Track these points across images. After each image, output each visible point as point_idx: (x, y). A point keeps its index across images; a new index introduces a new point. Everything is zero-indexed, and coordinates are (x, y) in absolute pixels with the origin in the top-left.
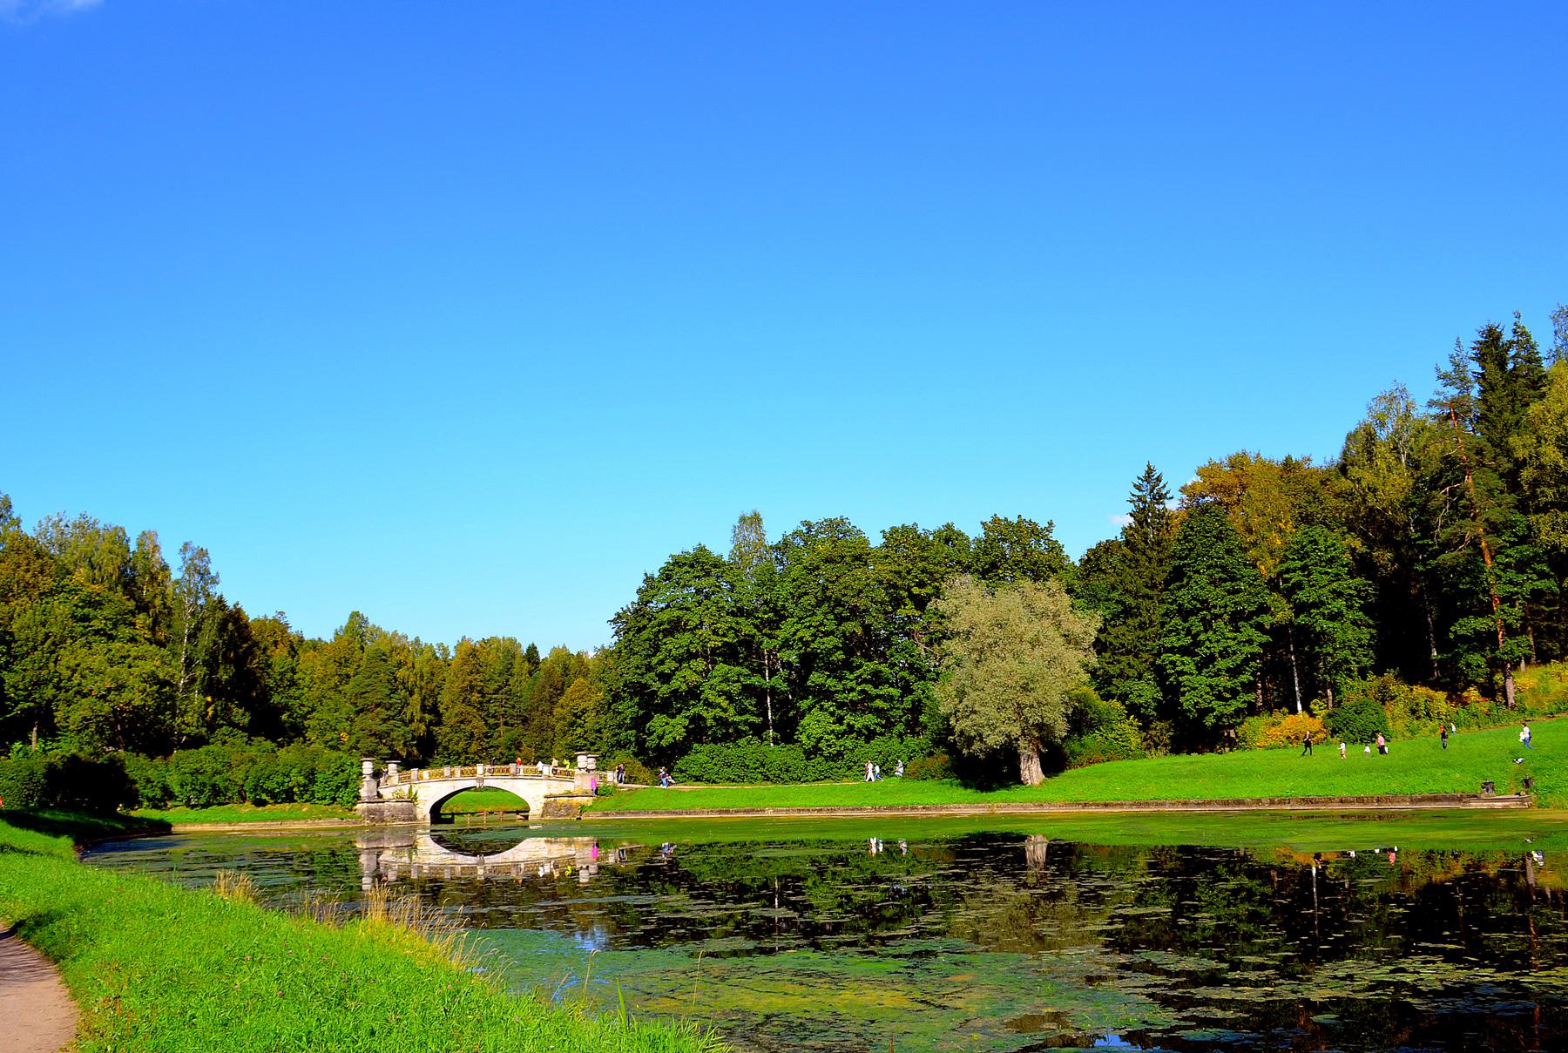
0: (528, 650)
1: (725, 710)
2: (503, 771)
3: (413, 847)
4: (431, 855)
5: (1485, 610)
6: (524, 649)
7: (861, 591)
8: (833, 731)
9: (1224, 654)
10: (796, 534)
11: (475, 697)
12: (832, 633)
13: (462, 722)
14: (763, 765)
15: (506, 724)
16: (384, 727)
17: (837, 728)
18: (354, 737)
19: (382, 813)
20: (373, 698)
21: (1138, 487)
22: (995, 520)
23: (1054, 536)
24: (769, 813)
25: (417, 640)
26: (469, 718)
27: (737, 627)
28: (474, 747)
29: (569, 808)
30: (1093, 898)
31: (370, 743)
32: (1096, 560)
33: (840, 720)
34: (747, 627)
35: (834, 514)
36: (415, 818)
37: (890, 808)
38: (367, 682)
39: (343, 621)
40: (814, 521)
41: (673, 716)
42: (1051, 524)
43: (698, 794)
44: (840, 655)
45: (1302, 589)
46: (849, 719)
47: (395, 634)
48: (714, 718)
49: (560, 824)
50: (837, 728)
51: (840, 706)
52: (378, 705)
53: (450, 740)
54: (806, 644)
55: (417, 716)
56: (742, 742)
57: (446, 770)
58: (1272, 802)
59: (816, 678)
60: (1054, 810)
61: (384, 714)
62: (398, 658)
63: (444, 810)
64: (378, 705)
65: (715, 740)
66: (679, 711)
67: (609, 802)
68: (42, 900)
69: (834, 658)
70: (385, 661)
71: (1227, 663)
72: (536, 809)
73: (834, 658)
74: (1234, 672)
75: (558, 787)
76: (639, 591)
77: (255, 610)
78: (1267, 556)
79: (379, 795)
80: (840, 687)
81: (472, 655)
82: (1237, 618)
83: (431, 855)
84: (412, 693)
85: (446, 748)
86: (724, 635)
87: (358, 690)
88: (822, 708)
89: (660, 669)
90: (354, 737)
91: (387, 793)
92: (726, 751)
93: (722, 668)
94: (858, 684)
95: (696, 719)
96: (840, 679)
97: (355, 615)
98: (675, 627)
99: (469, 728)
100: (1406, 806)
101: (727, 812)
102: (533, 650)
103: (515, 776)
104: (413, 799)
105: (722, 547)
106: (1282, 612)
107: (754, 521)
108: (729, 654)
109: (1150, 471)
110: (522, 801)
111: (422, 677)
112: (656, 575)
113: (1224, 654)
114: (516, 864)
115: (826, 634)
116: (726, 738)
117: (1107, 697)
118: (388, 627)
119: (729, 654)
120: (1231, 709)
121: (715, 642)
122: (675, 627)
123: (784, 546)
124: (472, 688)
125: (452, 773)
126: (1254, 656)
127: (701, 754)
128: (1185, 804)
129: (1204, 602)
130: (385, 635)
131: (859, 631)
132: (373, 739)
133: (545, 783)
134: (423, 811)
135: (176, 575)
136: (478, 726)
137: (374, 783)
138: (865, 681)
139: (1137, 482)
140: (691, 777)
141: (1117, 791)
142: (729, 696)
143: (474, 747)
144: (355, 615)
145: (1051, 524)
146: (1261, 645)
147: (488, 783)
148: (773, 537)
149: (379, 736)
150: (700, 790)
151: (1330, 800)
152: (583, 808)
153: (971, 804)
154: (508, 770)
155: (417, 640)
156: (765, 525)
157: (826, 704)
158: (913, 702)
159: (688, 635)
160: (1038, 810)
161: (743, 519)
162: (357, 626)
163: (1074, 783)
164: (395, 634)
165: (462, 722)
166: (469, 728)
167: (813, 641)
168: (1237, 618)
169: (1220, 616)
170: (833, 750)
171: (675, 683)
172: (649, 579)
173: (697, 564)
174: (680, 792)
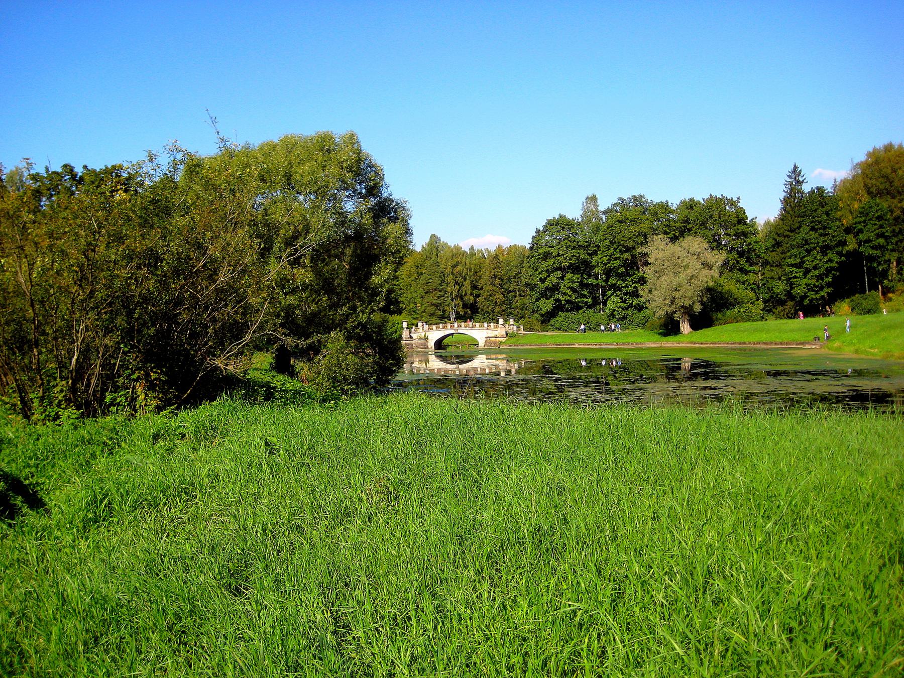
1: (570, 296)
3: (427, 361)
4: (436, 364)
5: (409, 328)
7: (630, 238)
8: (620, 307)
9: (815, 268)
10: (615, 205)
11: (497, 281)
12: (619, 258)
13: (490, 295)
14: (588, 323)
15: (520, 295)
16: (438, 301)
17: (623, 305)
18: (424, 306)
20: (432, 286)
21: (789, 177)
23: (741, 205)
24: (576, 346)
25: (472, 248)
26: (494, 293)
27: (577, 255)
28: (498, 309)
29: (495, 343)
31: (432, 309)
33: (624, 301)
34: (583, 255)
36: (428, 347)
37: (623, 344)
38: (429, 277)
39: (427, 240)
41: (548, 299)
43: (552, 337)
44: (622, 270)
45: (862, 233)
46: (630, 301)
48: (565, 300)
49: (492, 349)
50: (623, 305)
51: (626, 294)
52: (435, 289)
53: (484, 306)
54: (605, 264)
55: (469, 293)
56: (581, 311)
58: (754, 344)
59: (612, 281)
60: (683, 345)
61: (439, 294)
62: (456, 260)
63: (445, 341)
64: (435, 289)
65: (567, 311)
66: (551, 296)
67: (513, 340)
69: (619, 271)
70: (438, 266)
71: (816, 273)
72: (481, 343)
73: (619, 271)
74: (820, 277)
75: (491, 333)
76: (533, 237)
78: (848, 214)
79: (411, 337)
80: (624, 285)
82: (825, 249)
83: (436, 364)
84: (465, 280)
85: (482, 310)
86: (570, 259)
87: (425, 282)
88: (617, 295)
89: (541, 276)
90: (424, 306)
91: (415, 336)
92: (573, 316)
93: (569, 276)
94: (633, 283)
95: (558, 300)
96: (624, 281)
97: (433, 236)
98: (547, 256)
99: (494, 299)
100: (773, 346)
101: (560, 345)
103: (472, 328)
104: (426, 339)
105: (574, 213)
106: (852, 245)
107: (593, 199)
108: (574, 268)
109: (795, 167)
111: (470, 270)
112: (541, 229)
113: (815, 268)
114: (475, 370)
115: (615, 259)
116: (572, 310)
118: (451, 243)
119: (574, 268)
120: (818, 296)
121: (565, 264)
122: (547, 256)
123: (607, 212)
124: (496, 277)
126: (832, 269)
127: (561, 317)
128: (728, 344)
129: (806, 241)
130: (449, 247)
131: (630, 258)
132: (433, 307)
133: (486, 331)
134: (431, 344)
136: (499, 297)
138: (636, 282)
140: (557, 328)
141: (725, 337)
142: (572, 289)
143: (498, 309)
144: (433, 236)
146: (837, 263)
148: (602, 207)
149: (436, 306)
150: (553, 335)
151: (772, 343)
152: (501, 343)
153: (654, 342)
155: (472, 248)
156: (599, 202)
157: (619, 293)
159: (553, 260)
160: (678, 345)
161: (588, 198)
163: (708, 336)
165: (490, 295)
166: (494, 299)
167: (609, 263)
168: (825, 249)
169: (815, 248)
170: (621, 316)
171: (547, 283)
172: (538, 231)
173: (559, 224)
174: (545, 335)
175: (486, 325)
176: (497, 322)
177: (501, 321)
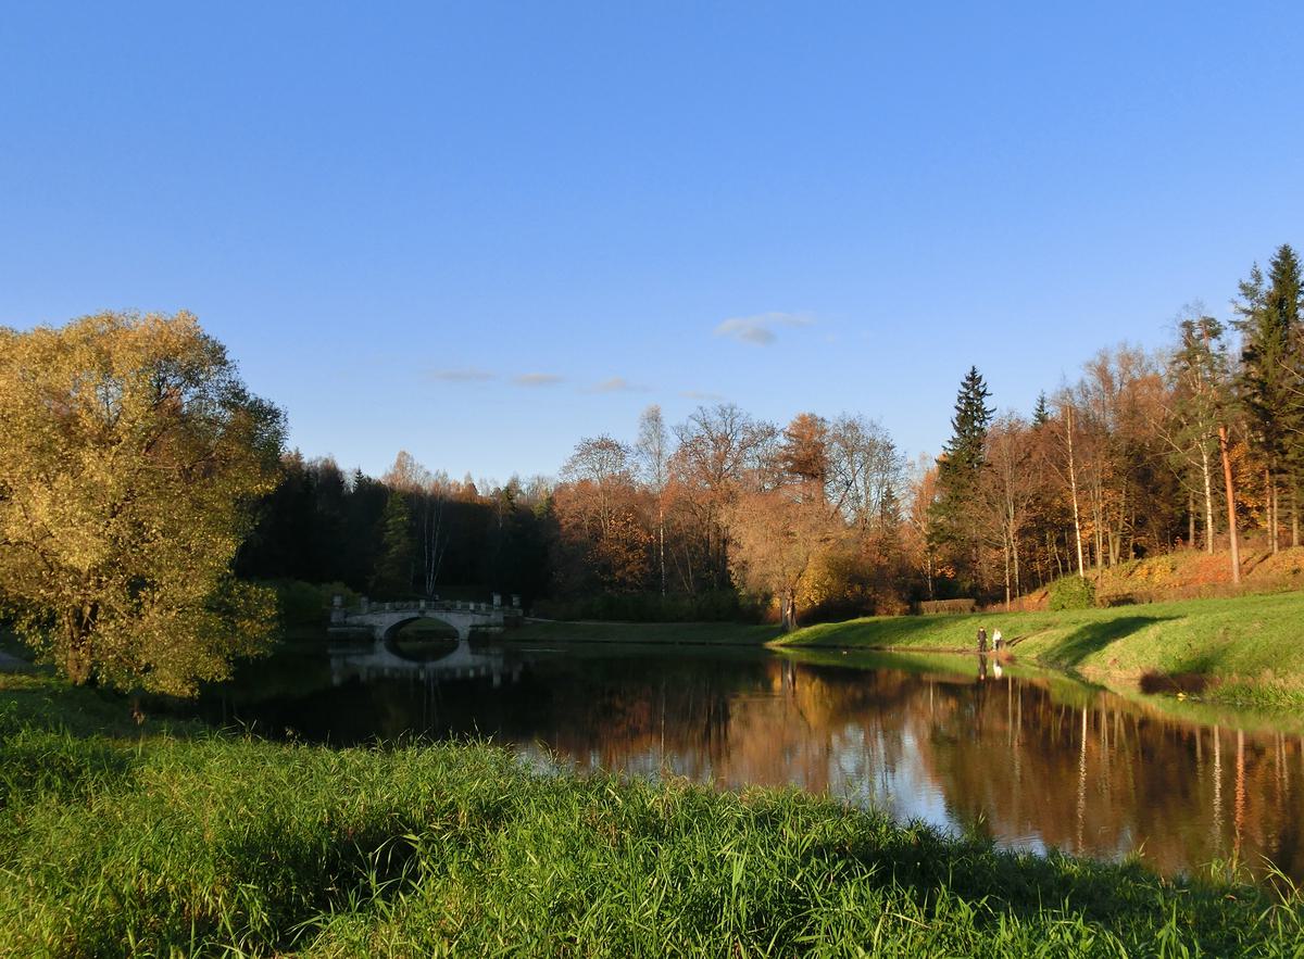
75: (479, 620)
103: (448, 610)
175: (472, 606)
176: (490, 601)
177: (497, 599)
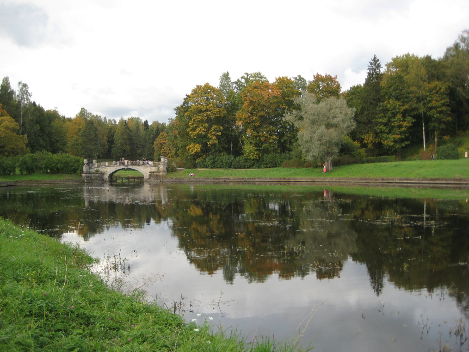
0: (145, 122)
2: (134, 163)
6: (143, 122)
19: (91, 177)
22: (318, 75)
23: (337, 80)
30: (297, 114)
32: (355, 91)
35: (257, 71)
40: (249, 73)
42: (336, 76)
47: (97, 116)
57: (114, 162)
68: (150, 304)
75: (154, 169)
77: (47, 107)
81: (125, 124)
102: (146, 122)
103: (139, 165)
105: (216, 84)
109: (375, 57)
110: (144, 176)
117: (354, 140)
125: (116, 164)
134: (106, 177)
135: (17, 93)
137: (88, 167)
139: (371, 61)
144: (83, 109)
145: (336, 76)
147: (130, 167)
154: (136, 163)
158: (317, 199)
162: (83, 112)
164: (97, 116)
